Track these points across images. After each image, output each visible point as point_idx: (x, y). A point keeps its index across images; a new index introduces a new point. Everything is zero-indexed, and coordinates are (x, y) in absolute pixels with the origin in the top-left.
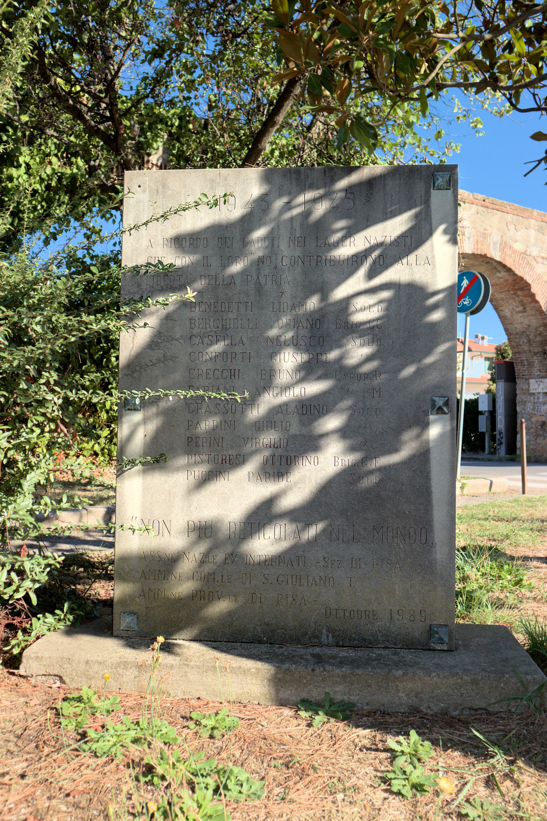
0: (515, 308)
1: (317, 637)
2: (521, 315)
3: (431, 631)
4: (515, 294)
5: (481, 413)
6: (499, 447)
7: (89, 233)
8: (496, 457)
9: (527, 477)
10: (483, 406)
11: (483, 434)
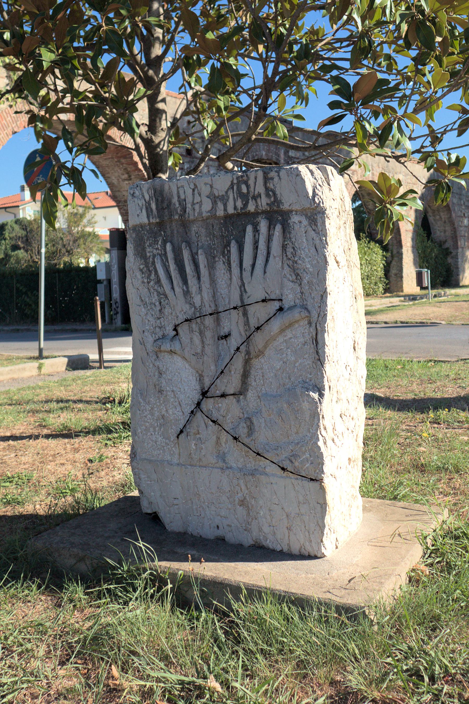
0: (121, 176)
2: (127, 182)
4: (119, 161)
5: (100, 282)
6: (115, 317)
8: (113, 327)
10: (101, 275)
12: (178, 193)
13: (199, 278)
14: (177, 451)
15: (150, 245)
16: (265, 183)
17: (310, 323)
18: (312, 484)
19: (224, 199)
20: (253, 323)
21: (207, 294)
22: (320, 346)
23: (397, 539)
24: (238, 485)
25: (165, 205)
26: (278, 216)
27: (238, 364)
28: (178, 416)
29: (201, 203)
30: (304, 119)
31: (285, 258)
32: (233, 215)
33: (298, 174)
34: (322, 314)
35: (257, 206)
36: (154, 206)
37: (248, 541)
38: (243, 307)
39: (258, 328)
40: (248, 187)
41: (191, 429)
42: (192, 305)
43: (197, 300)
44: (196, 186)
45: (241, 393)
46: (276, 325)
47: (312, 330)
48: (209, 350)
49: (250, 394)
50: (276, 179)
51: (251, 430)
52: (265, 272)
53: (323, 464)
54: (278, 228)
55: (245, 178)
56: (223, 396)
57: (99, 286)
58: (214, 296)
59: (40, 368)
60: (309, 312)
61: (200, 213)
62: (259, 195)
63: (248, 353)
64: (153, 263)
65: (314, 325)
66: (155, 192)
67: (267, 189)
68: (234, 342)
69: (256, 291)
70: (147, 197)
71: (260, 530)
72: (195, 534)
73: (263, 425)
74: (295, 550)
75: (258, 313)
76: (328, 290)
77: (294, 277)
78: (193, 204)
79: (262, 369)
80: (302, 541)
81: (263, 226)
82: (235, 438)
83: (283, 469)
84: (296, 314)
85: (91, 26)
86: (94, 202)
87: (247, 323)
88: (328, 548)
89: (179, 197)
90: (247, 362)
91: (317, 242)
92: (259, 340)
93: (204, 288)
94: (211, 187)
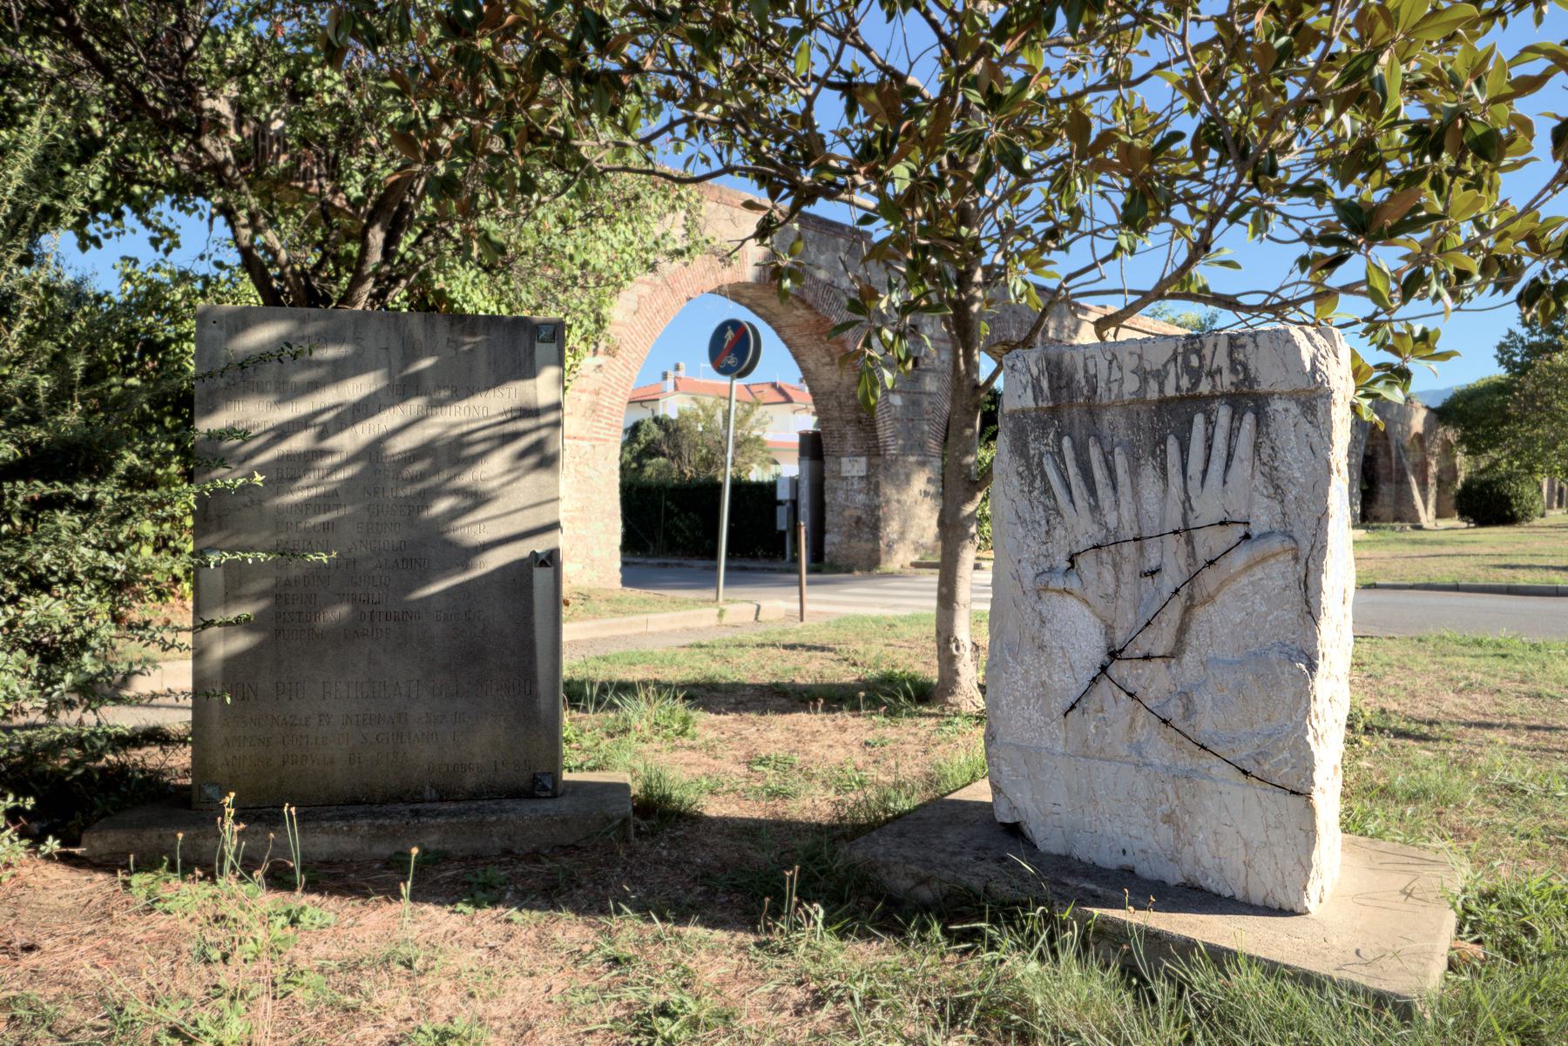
1: (420, 793)
3: (535, 780)
5: (781, 503)
7: (157, 235)
9: (806, 596)
10: (783, 494)
11: (783, 533)
12: (1085, 365)
13: (1115, 488)
14: (1062, 736)
15: (1036, 439)
16: (1230, 354)
17: (1296, 559)
18: (1291, 799)
19: (1160, 375)
20: (1202, 554)
21: (1127, 511)
22: (1311, 592)
24: (1163, 791)
25: (1063, 383)
28: (1069, 684)
30: (1238, 267)
31: (1257, 463)
32: (1173, 399)
35: (1214, 386)
36: (1045, 384)
37: (1174, 876)
38: (1186, 531)
39: (1211, 563)
40: (1201, 358)
41: (1091, 704)
42: (1103, 525)
43: (1111, 519)
44: (1114, 356)
46: (1240, 558)
47: (1300, 568)
48: (1126, 591)
49: (1187, 658)
50: (1250, 347)
51: (1189, 711)
52: (1225, 483)
53: (1313, 770)
54: (1249, 418)
56: (1147, 657)
57: (779, 508)
58: (1137, 514)
59: (721, 615)
61: (1120, 395)
62: (1220, 371)
63: (1191, 597)
64: (1040, 464)
66: (1048, 363)
67: (1233, 362)
68: (1170, 579)
69: (1208, 507)
70: (1035, 371)
71: (1197, 862)
72: (1084, 858)
73: (1209, 704)
74: (1257, 897)
75: (1210, 542)
76: (1330, 512)
77: (1271, 491)
78: (1109, 382)
79: (1209, 621)
80: (1269, 886)
81: (1223, 414)
82: (1165, 721)
83: (1245, 772)
84: (1275, 544)
86: (759, 396)
87: (1192, 554)
89: (1086, 371)
90: (1188, 610)
91: (1315, 439)
92: (1210, 578)
93: (1123, 502)
94: (1140, 357)
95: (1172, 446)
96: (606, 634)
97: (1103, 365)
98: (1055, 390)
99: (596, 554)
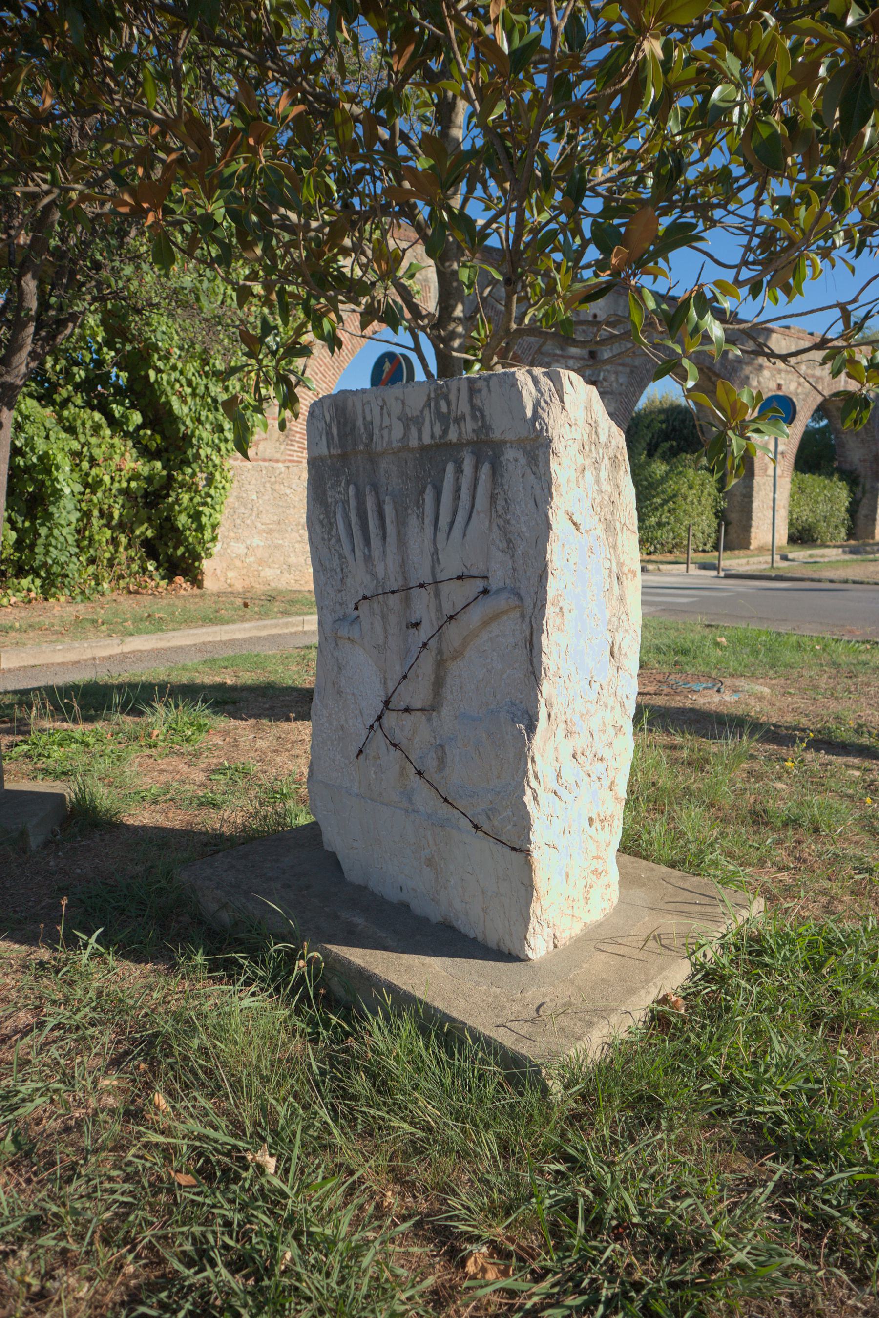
13: (384, 538)
15: (332, 488)
17: (523, 616)
19: (418, 421)
20: (448, 610)
22: (535, 652)
23: (651, 944)
26: (487, 450)
27: (427, 665)
29: (389, 428)
32: (430, 446)
33: (511, 382)
34: (539, 604)
35: (460, 434)
36: (335, 431)
39: (451, 617)
40: (449, 404)
42: (374, 576)
43: (380, 570)
45: (431, 709)
46: (475, 615)
47: (526, 626)
49: (446, 711)
50: (485, 392)
53: (530, 829)
54: (486, 468)
55: (445, 390)
56: (407, 710)
60: (521, 598)
61: (390, 442)
62: (463, 417)
63: (440, 652)
65: (527, 619)
67: (473, 407)
68: (424, 632)
75: (455, 595)
83: (476, 827)
84: (502, 602)
85: (590, 220)
87: (439, 609)
88: (538, 947)
90: (440, 664)
91: (538, 492)
92: (454, 633)
94: (403, 403)
95: (429, 496)
96: (264, 633)
97: (377, 410)
98: (342, 436)
99: (293, 559)
